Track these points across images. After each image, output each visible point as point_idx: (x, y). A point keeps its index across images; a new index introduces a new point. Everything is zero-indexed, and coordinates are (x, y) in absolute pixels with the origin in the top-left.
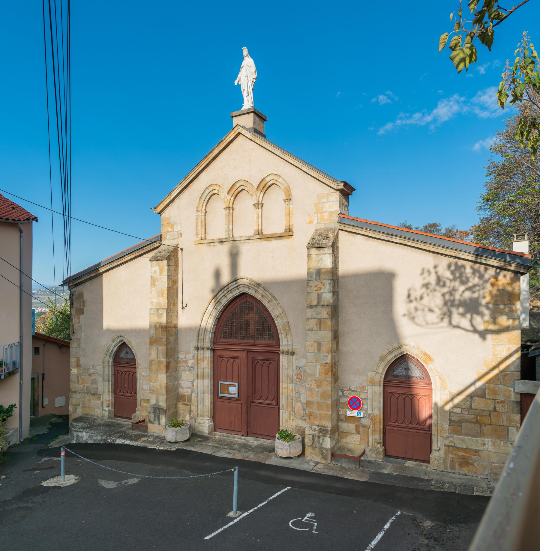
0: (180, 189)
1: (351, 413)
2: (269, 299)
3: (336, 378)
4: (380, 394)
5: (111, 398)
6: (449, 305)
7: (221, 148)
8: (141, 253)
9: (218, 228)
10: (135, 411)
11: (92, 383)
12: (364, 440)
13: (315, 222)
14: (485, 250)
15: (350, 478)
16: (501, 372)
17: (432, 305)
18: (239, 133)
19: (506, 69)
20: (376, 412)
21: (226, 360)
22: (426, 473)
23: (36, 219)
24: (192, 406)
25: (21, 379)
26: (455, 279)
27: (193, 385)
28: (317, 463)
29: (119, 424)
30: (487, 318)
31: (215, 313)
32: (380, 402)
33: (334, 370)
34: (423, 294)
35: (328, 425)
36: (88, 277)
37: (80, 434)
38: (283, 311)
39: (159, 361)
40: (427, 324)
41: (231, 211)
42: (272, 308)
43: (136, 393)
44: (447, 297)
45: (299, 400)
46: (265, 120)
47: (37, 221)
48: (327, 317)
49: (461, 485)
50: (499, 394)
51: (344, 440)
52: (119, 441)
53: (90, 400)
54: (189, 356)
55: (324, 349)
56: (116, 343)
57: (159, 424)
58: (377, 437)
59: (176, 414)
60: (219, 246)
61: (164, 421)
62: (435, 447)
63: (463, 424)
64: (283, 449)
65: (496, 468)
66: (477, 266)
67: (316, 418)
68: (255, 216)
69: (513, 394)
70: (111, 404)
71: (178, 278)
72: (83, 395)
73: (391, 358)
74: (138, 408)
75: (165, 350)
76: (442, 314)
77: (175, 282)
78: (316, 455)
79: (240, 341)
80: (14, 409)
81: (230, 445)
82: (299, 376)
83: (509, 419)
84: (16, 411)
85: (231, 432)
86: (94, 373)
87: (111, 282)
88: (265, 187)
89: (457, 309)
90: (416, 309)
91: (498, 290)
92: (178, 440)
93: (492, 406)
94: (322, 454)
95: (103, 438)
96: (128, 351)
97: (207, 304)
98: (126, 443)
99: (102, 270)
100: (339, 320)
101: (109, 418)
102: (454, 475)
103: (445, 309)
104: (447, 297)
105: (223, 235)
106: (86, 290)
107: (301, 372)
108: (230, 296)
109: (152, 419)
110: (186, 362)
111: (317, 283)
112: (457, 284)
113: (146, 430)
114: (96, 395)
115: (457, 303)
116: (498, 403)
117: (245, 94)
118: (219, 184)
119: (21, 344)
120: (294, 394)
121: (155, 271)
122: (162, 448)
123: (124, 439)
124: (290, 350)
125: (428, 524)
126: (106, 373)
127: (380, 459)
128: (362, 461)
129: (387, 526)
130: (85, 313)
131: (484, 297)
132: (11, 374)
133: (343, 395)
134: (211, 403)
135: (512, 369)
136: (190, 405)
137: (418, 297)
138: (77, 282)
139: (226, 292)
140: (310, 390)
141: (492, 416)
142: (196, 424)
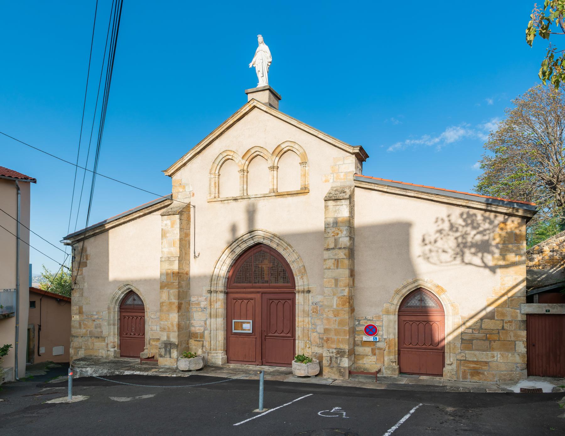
0: (193, 154)
1: (366, 338)
2: (285, 247)
3: (352, 310)
4: (395, 322)
5: (116, 340)
6: (462, 247)
7: (235, 119)
8: (150, 210)
9: (232, 185)
10: (143, 350)
11: (96, 328)
12: (380, 359)
13: (331, 181)
14: (495, 200)
15: (368, 388)
16: (509, 298)
17: (446, 247)
18: (255, 107)
19: (535, 11)
20: (392, 337)
21: (240, 301)
22: (440, 383)
23: (34, 181)
25: (17, 323)
26: (467, 225)
27: (206, 324)
28: (335, 380)
29: (125, 361)
30: (497, 255)
31: (229, 262)
32: (395, 329)
33: (351, 302)
34: (437, 238)
35: (346, 347)
36: (91, 233)
37: (84, 370)
38: (299, 257)
39: (170, 303)
40: (441, 262)
41: (246, 174)
42: (287, 255)
43: (144, 334)
44: (460, 240)
46: (280, 99)
47: (35, 182)
48: (345, 257)
49: (473, 389)
50: (507, 316)
51: (360, 362)
52: (127, 373)
53: (93, 343)
54: (203, 299)
55: (341, 284)
56: (122, 291)
57: (170, 357)
58: (392, 357)
59: (188, 348)
60: (233, 203)
61: (176, 355)
62: (447, 361)
63: (474, 341)
64: (300, 370)
65: (505, 375)
66: (487, 214)
67: (333, 342)
68: (271, 177)
69: (519, 315)
70: (116, 345)
71: (190, 232)
72: (86, 338)
73: (405, 292)
74: (147, 346)
75: (177, 293)
76: (455, 254)
77: (188, 235)
78: (334, 373)
79: (254, 285)
80: (10, 349)
81: (246, 372)
82: (315, 310)
83: (516, 336)
84: (12, 351)
85: (245, 363)
86: (98, 319)
87: (116, 237)
88: (280, 152)
89: (470, 249)
90: (431, 251)
91: (507, 233)
93: (501, 325)
94: (340, 372)
95: (110, 371)
96: (136, 297)
98: (135, 373)
99: (107, 226)
100: (355, 261)
101: (115, 357)
102: (466, 383)
103: (458, 250)
104: (460, 240)
105: (237, 193)
106: (91, 245)
108: (244, 246)
109: (163, 353)
110: (199, 304)
111: (334, 229)
112: (469, 229)
113: (157, 364)
114: (100, 337)
115: (469, 244)
116: (506, 323)
117: (259, 75)
118: (233, 150)
119: (17, 291)
120: (310, 326)
121: (166, 225)
122: (175, 376)
123: (133, 370)
124: (306, 289)
125: (450, 409)
126: (112, 318)
127: (396, 375)
128: (379, 377)
129: (412, 411)
130: (88, 265)
131: (494, 239)
132: (6, 317)
133: (359, 324)
134: (224, 338)
135: (519, 295)
137: (433, 241)
138: (80, 238)
139: (240, 242)
140: (328, 319)
141: (501, 334)
142: (209, 357)
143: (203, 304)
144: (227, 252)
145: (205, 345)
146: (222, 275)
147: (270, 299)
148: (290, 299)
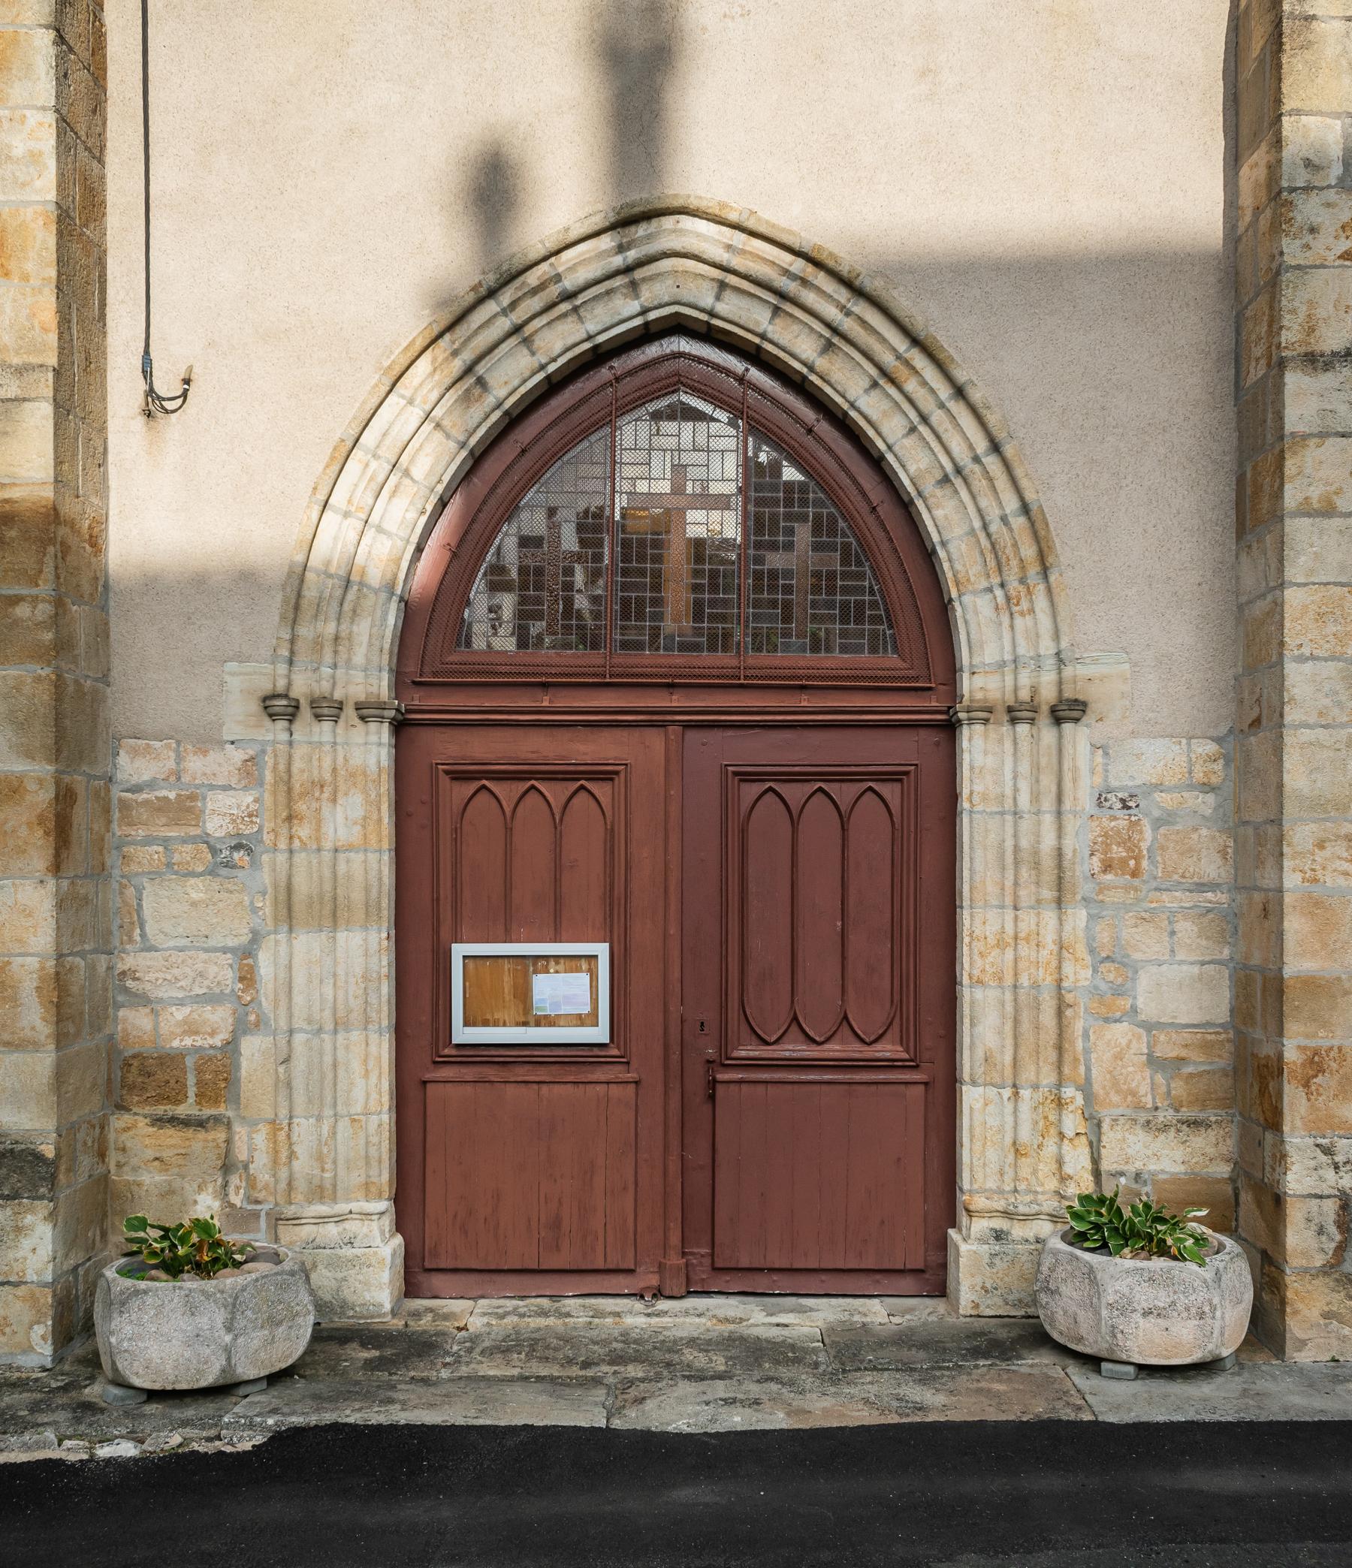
24: (240, 1131)
27: (248, 977)
31: (434, 460)
45: (1125, 1003)
79: (624, 659)
82: (1118, 852)
92: (247, 1370)
97: (372, 381)
107: (1133, 825)
108: (560, 340)
110: (185, 809)
122: (126, 1449)
124: (1048, 694)
136: (229, 1125)
139: (535, 303)
143: (223, 813)
144: (427, 377)
145: (241, 1153)
146: (375, 576)
147: (746, 777)
148: (894, 777)
